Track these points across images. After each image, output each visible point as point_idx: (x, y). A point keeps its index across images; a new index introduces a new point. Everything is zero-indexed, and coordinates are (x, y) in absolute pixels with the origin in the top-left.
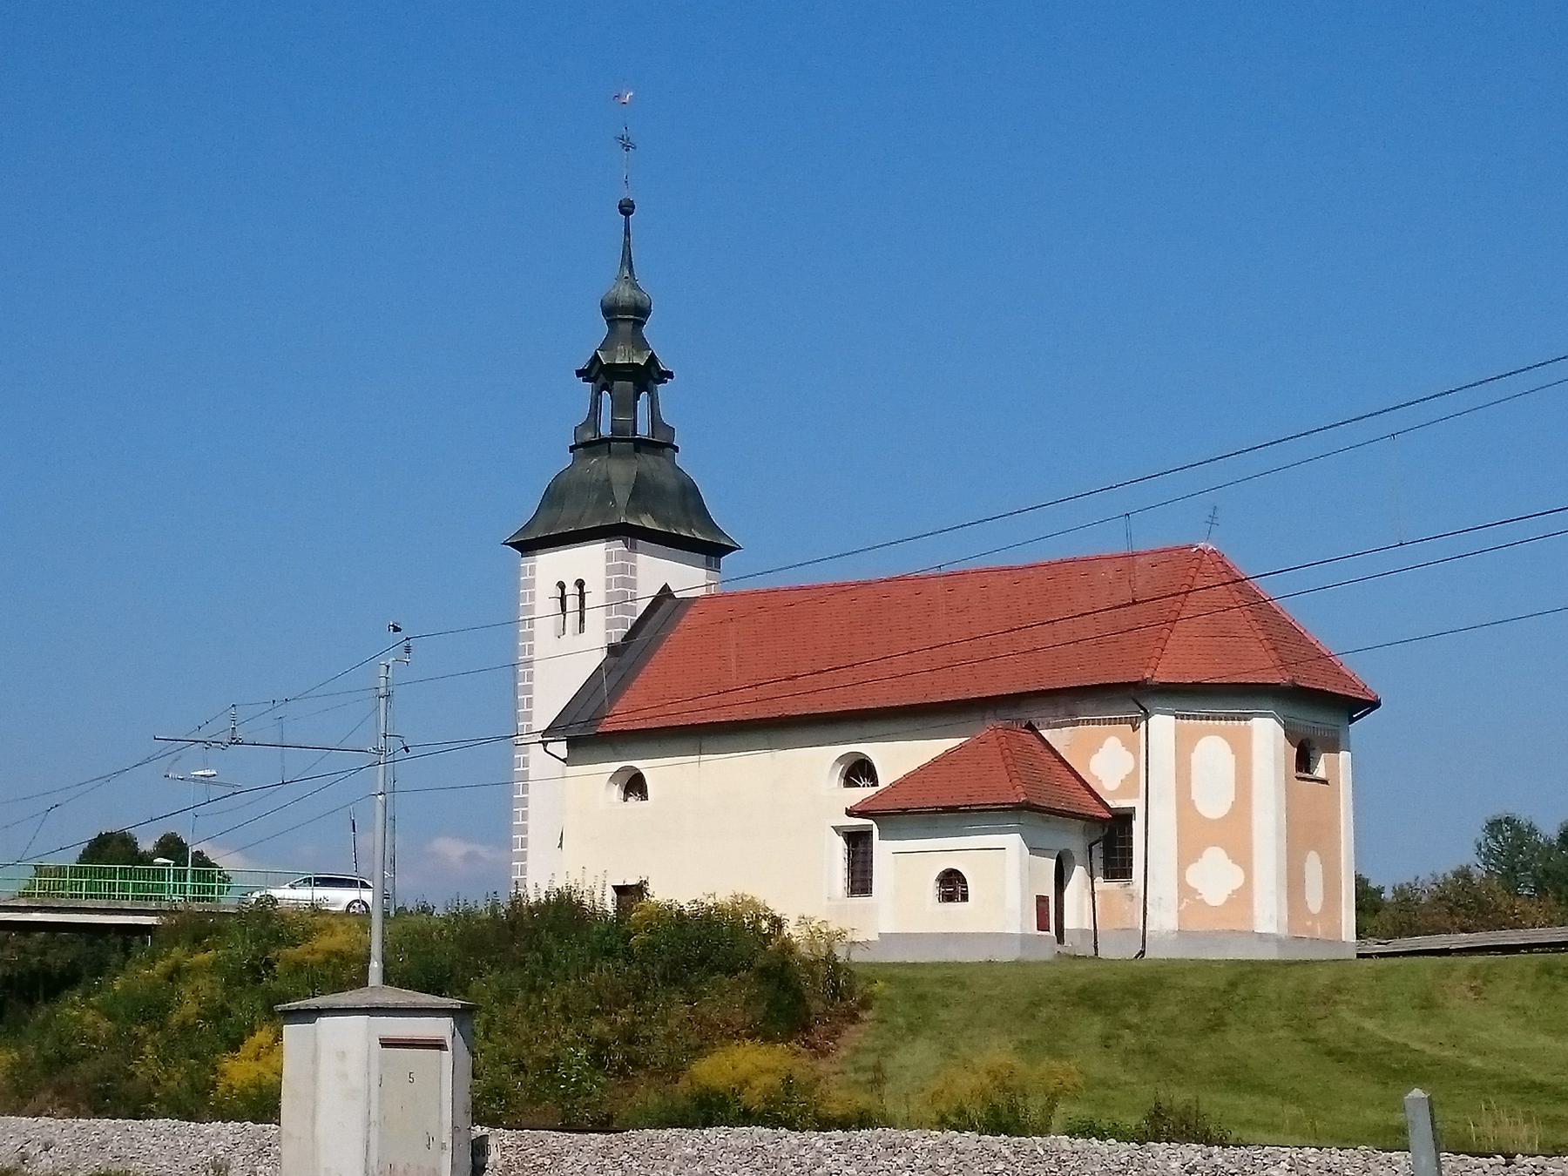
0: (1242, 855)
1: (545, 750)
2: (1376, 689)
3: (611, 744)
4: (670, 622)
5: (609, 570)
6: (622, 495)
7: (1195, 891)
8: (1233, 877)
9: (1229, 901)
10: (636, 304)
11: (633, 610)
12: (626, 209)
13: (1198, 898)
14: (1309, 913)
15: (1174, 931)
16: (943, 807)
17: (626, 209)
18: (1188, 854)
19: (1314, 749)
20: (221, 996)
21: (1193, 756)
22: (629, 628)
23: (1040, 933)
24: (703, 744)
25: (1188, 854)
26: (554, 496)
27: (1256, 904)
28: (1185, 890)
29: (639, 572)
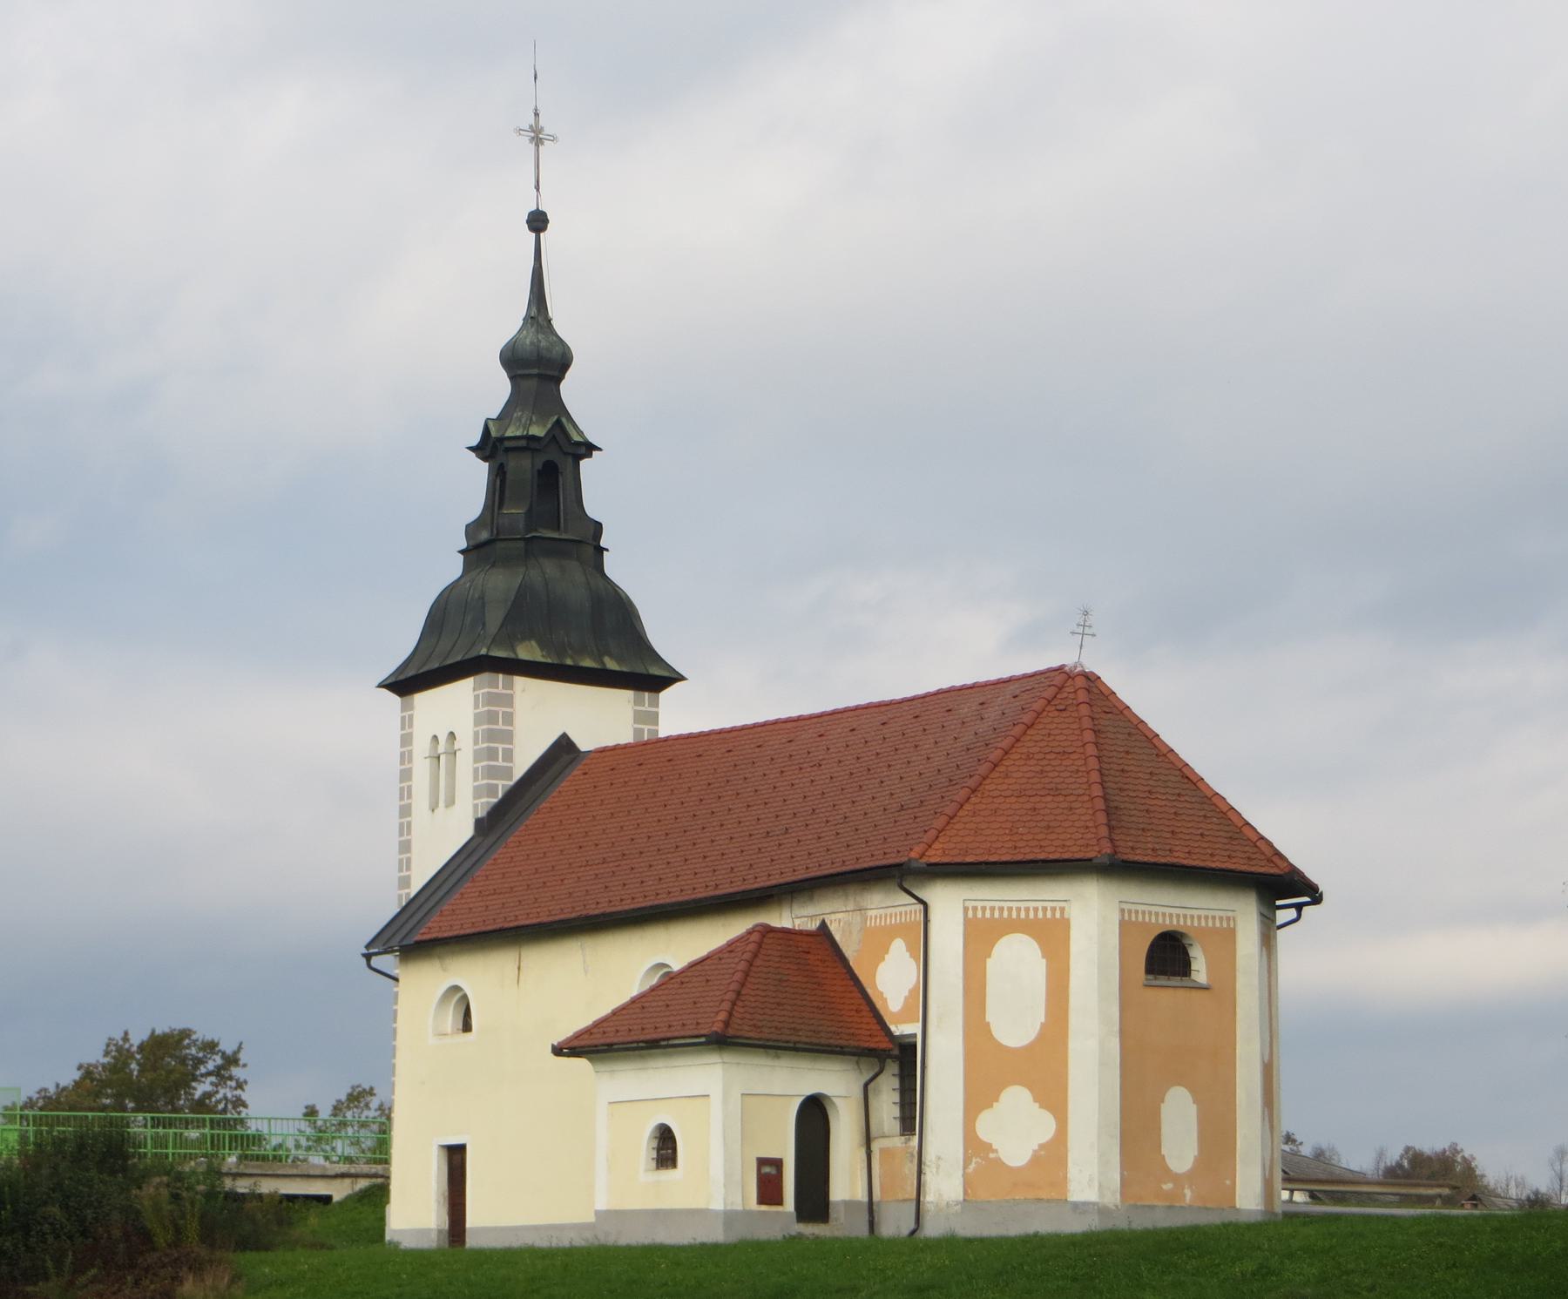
0: (1053, 1097)
1: (369, 966)
2: (361, 956)
3: (439, 957)
4: (569, 783)
5: (477, 722)
6: (494, 618)
7: (988, 1147)
8: (1042, 1127)
9: (1036, 1160)
10: (538, 351)
11: (508, 772)
12: (538, 222)
13: (992, 1155)
14: (1167, 1170)
15: (957, 1203)
16: (646, 1042)
17: (538, 222)
18: (978, 1097)
19: (1191, 945)
20: (1314, 1245)
21: (989, 962)
22: (500, 795)
23: (764, 1208)
24: (522, 954)
25: (978, 1097)
26: (441, 617)
27: (1070, 1164)
28: (974, 1145)
29: (518, 720)
